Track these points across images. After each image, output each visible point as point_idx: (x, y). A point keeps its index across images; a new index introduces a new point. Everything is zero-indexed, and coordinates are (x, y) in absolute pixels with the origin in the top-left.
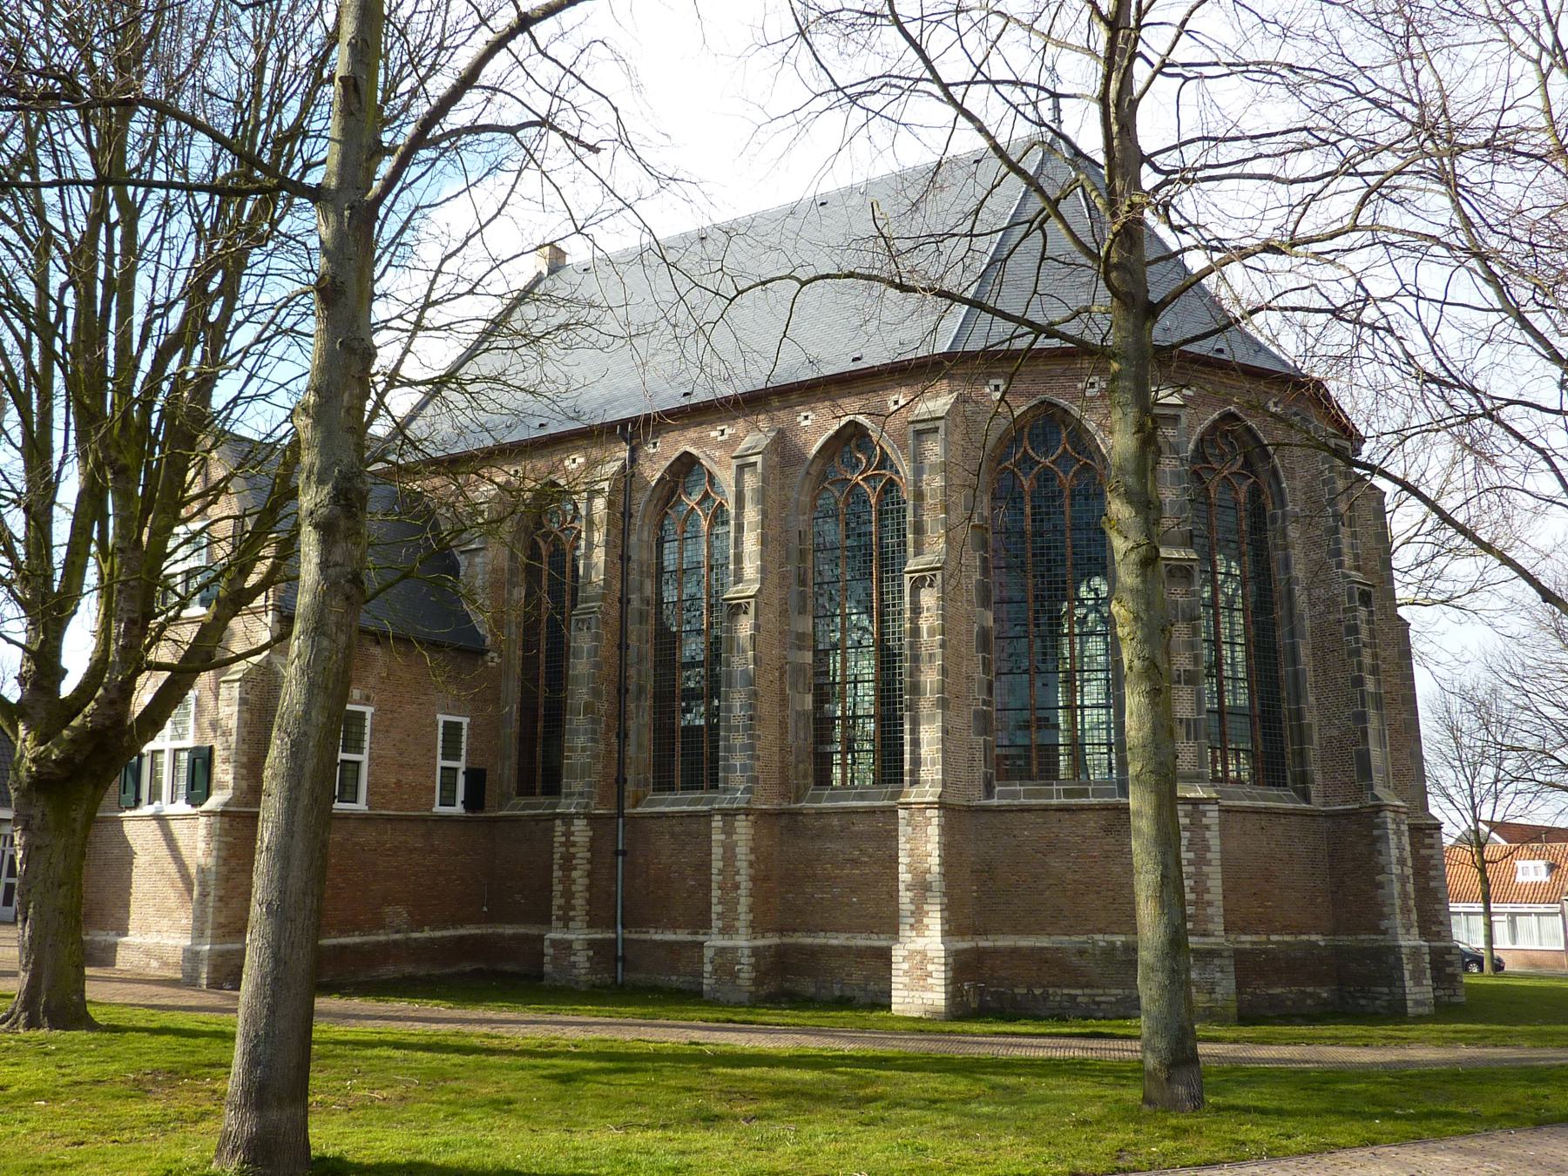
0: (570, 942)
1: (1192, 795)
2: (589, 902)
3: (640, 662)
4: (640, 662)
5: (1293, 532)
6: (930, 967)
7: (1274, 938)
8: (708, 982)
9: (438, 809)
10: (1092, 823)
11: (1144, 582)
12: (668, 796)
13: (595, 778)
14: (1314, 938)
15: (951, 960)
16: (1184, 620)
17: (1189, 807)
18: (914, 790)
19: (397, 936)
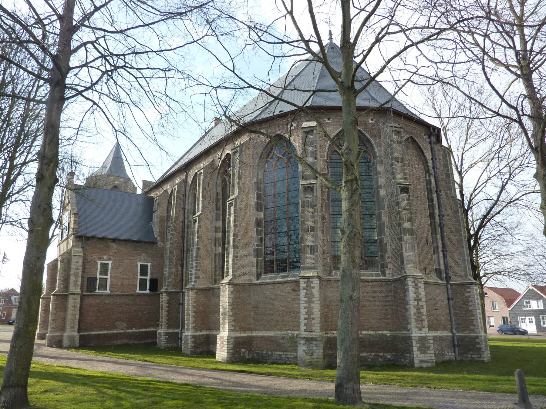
1: (307, 275)
2: (168, 320)
9: (138, 291)
10: (289, 287)
14: (385, 332)
16: (311, 207)
17: (306, 280)
19: (121, 331)
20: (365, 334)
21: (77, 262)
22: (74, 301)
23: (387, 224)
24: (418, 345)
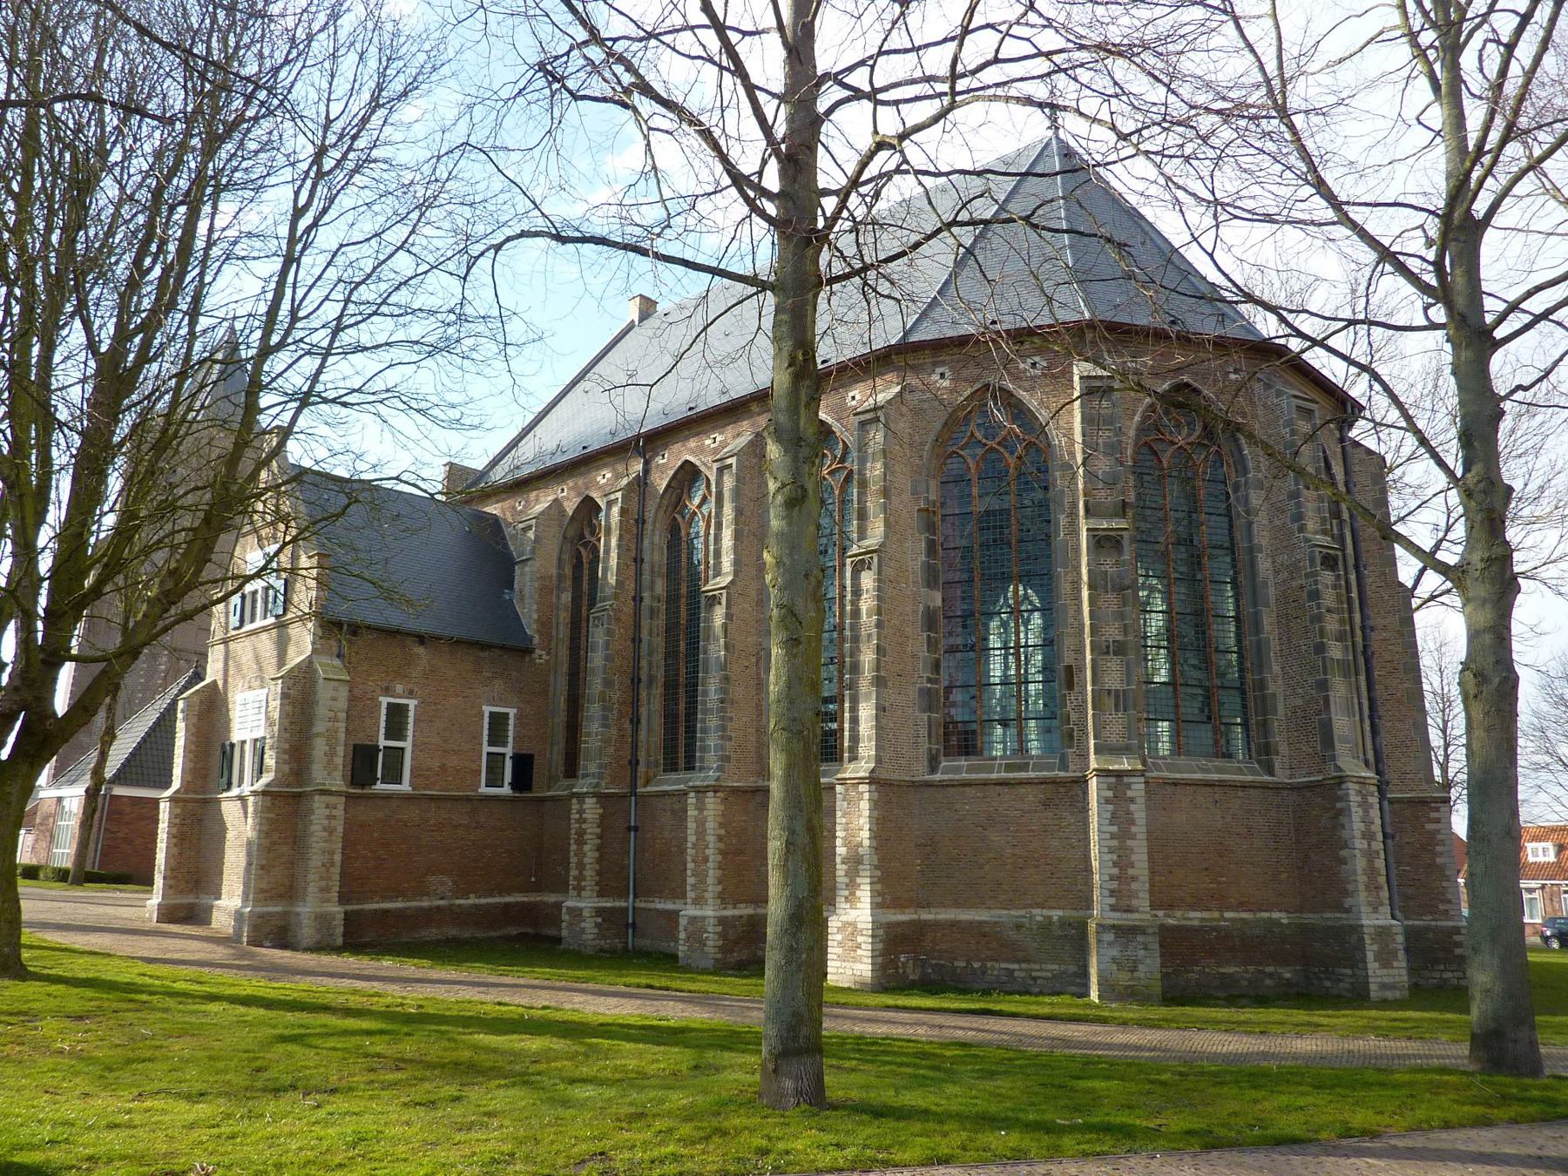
0: (581, 909)
1: (1116, 767)
2: (599, 873)
3: (650, 654)
4: (650, 654)
5: (1256, 498)
6: (860, 939)
7: (1228, 915)
8: (682, 949)
11: (790, 524)
12: (673, 776)
13: (606, 760)
14: (1276, 915)
15: (881, 932)
16: (1113, 589)
17: (1113, 780)
18: (852, 766)
19: (441, 903)
20: (1232, 920)
21: (334, 699)
22: (327, 812)
23: (1274, 645)
24: (1375, 947)
